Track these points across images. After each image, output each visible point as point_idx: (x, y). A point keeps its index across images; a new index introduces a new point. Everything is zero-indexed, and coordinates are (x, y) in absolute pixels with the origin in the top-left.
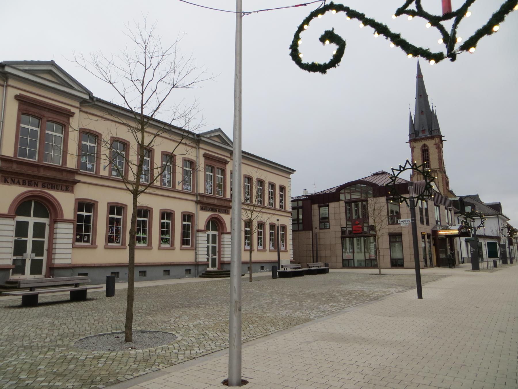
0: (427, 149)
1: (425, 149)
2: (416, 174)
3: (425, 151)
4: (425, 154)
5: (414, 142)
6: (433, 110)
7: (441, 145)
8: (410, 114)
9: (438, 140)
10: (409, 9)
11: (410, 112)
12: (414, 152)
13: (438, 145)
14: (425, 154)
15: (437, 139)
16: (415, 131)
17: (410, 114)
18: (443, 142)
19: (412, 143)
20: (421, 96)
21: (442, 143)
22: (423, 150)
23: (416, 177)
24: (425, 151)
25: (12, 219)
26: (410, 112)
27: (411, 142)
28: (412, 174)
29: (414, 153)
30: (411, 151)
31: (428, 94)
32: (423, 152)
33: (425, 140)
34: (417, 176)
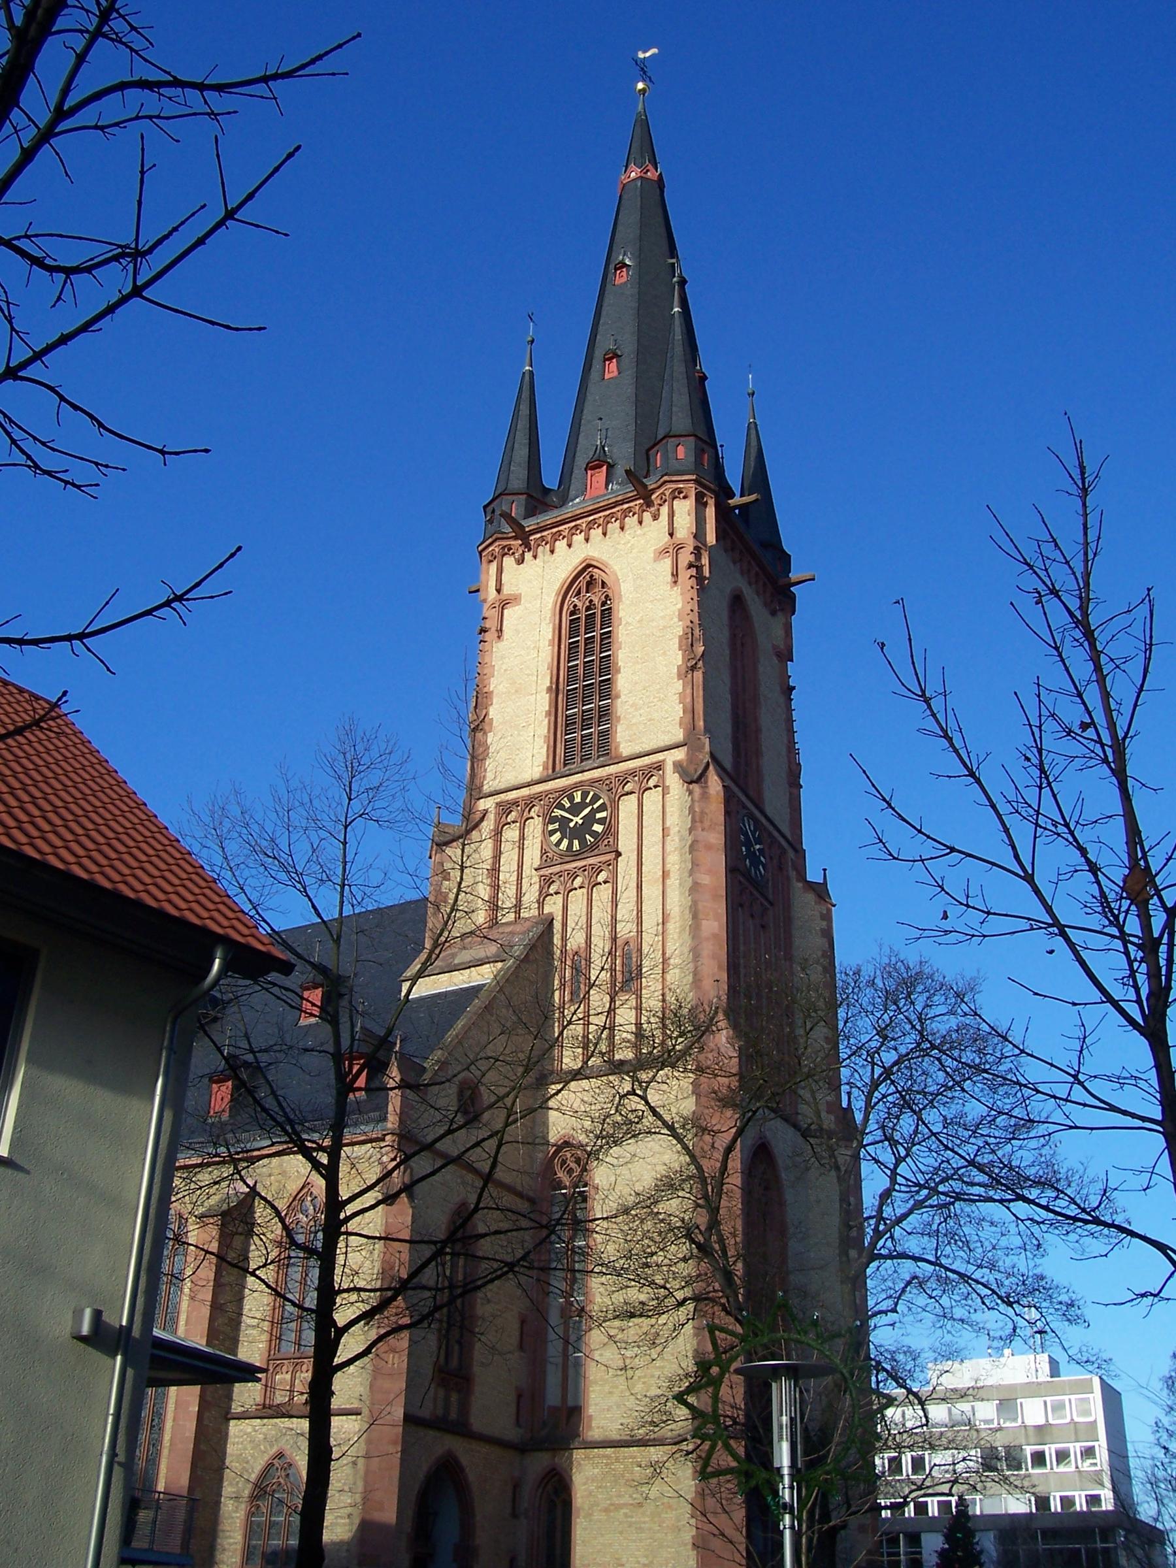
32: (573, 631)
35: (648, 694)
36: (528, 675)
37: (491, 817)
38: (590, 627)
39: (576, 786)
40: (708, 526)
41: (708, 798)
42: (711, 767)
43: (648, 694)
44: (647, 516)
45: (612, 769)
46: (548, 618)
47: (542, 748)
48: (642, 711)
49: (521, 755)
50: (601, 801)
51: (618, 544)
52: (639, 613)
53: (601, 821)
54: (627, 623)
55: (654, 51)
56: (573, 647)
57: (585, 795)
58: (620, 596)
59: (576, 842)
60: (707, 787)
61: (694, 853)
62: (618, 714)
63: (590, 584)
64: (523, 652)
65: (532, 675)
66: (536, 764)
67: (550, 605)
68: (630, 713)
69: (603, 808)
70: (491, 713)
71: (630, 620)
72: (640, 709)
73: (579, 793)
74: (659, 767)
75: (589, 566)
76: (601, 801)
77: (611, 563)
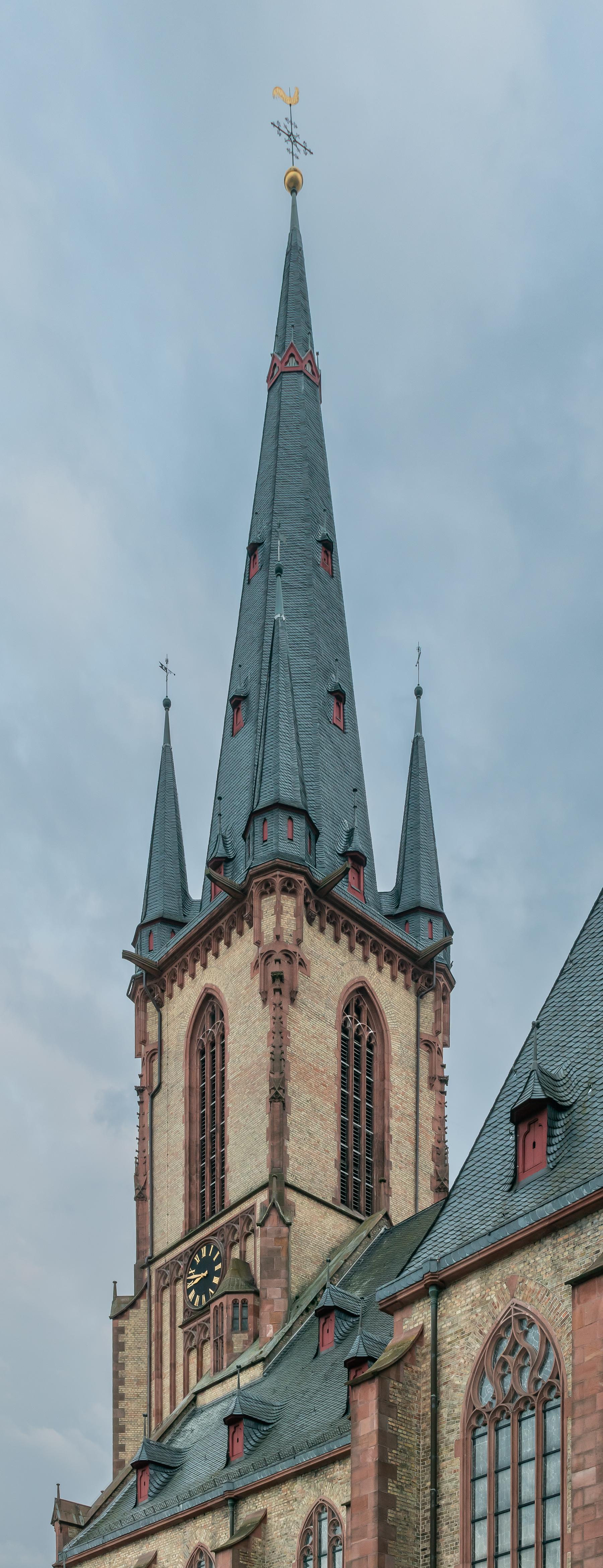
28: (128, 1290)
53: (217, 1274)
59: (204, 1297)
74: (252, 1210)
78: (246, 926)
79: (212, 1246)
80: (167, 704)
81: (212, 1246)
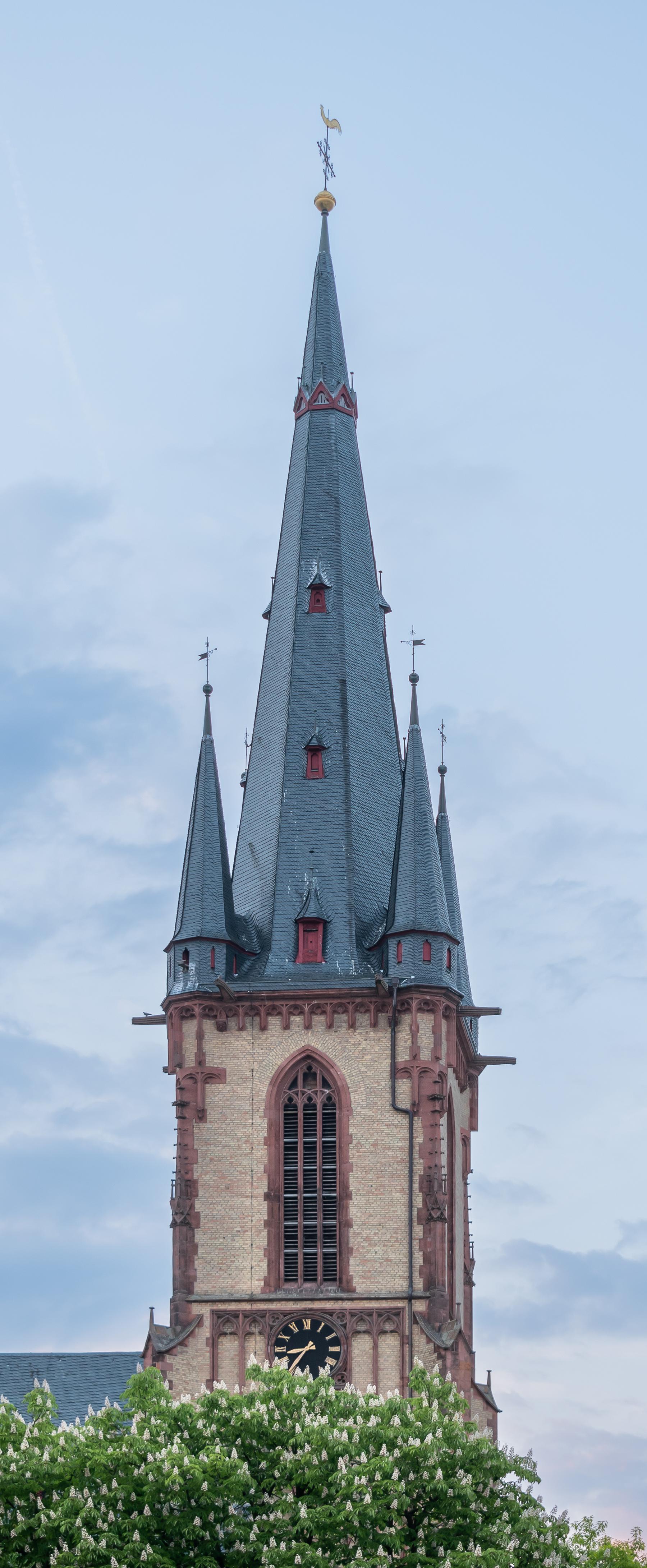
0: (330, 1103)
1: (310, 1105)
2: (205, 1332)
3: (310, 1118)
4: (309, 1159)
5: (209, 1026)
6: (415, 734)
7: (460, 1101)
8: (207, 747)
9: (435, 1031)
10: (325, 1494)
11: (208, 729)
12: (202, 1115)
13: (427, 1081)
14: (309, 1159)
15: (425, 1021)
16: (234, 922)
17: (207, 747)
18: (487, 1077)
19: (190, 1028)
20: (315, 750)
21: (469, 1083)
22: (290, 1105)
23: (207, 1352)
24: (310, 1118)
25: (328, 925)
26: (208, 729)
27: (187, 1015)
28: (164, 1319)
29: (201, 1130)
30: (180, 1105)
31: (388, 595)
32: (290, 1128)
33: (319, 1020)
34: (213, 1343)
35: (384, 1231)
36: (241, 1173)
37: (207, 1322)
38: (309, 1130)
39: (306, 1313)
40: (443, 1028)
41: (458, 1365)
42: (418, 1000)
43: (384, 1231)
44: (383, 1018)
45: (347, 1305)
46: (261, 1111)
47: (261, 1261)
48: (377, 1248)
49: (236, 1263)
50: (334, 1335)
51: (347, 1042)
52: (372, 1135)
54: (359, 1143)
55: (319, 1331)
56: (290, 1149)
57: (315, 1324)
58: (350, 1110)
60: (457, 1354)
61: (378, 984)
62: (351, 1245)
63: (310, 1075)
64: (232, 1144)
65: (246, 1173)
66: (256, 1277)
67: (264, 1095)
68: (363, 1247)
69: (336, 1342)
70: (197, 1206)
71: (363, 1141)
72: (375, 1245)
73: (309, 1322)
75: (308, 1057)
76: (334, 1335)
77: (339, 1064)
78: (383, 1018)
79: (323, 1324)
80: (207, 690)
81: (323, 1324)
